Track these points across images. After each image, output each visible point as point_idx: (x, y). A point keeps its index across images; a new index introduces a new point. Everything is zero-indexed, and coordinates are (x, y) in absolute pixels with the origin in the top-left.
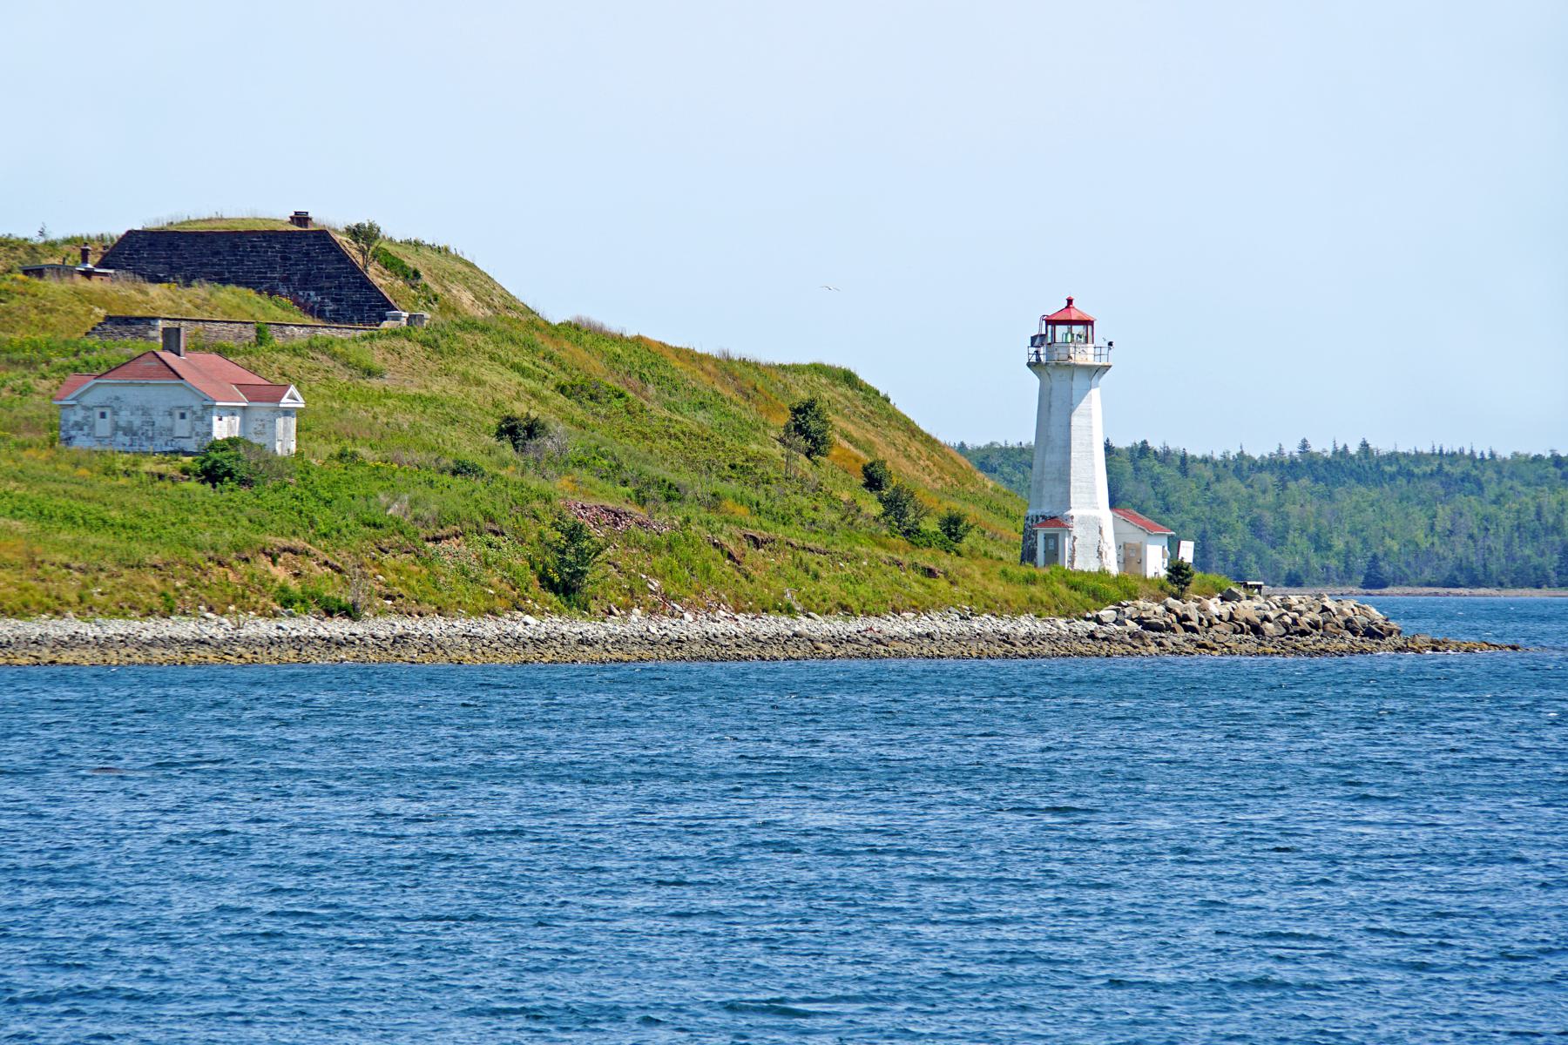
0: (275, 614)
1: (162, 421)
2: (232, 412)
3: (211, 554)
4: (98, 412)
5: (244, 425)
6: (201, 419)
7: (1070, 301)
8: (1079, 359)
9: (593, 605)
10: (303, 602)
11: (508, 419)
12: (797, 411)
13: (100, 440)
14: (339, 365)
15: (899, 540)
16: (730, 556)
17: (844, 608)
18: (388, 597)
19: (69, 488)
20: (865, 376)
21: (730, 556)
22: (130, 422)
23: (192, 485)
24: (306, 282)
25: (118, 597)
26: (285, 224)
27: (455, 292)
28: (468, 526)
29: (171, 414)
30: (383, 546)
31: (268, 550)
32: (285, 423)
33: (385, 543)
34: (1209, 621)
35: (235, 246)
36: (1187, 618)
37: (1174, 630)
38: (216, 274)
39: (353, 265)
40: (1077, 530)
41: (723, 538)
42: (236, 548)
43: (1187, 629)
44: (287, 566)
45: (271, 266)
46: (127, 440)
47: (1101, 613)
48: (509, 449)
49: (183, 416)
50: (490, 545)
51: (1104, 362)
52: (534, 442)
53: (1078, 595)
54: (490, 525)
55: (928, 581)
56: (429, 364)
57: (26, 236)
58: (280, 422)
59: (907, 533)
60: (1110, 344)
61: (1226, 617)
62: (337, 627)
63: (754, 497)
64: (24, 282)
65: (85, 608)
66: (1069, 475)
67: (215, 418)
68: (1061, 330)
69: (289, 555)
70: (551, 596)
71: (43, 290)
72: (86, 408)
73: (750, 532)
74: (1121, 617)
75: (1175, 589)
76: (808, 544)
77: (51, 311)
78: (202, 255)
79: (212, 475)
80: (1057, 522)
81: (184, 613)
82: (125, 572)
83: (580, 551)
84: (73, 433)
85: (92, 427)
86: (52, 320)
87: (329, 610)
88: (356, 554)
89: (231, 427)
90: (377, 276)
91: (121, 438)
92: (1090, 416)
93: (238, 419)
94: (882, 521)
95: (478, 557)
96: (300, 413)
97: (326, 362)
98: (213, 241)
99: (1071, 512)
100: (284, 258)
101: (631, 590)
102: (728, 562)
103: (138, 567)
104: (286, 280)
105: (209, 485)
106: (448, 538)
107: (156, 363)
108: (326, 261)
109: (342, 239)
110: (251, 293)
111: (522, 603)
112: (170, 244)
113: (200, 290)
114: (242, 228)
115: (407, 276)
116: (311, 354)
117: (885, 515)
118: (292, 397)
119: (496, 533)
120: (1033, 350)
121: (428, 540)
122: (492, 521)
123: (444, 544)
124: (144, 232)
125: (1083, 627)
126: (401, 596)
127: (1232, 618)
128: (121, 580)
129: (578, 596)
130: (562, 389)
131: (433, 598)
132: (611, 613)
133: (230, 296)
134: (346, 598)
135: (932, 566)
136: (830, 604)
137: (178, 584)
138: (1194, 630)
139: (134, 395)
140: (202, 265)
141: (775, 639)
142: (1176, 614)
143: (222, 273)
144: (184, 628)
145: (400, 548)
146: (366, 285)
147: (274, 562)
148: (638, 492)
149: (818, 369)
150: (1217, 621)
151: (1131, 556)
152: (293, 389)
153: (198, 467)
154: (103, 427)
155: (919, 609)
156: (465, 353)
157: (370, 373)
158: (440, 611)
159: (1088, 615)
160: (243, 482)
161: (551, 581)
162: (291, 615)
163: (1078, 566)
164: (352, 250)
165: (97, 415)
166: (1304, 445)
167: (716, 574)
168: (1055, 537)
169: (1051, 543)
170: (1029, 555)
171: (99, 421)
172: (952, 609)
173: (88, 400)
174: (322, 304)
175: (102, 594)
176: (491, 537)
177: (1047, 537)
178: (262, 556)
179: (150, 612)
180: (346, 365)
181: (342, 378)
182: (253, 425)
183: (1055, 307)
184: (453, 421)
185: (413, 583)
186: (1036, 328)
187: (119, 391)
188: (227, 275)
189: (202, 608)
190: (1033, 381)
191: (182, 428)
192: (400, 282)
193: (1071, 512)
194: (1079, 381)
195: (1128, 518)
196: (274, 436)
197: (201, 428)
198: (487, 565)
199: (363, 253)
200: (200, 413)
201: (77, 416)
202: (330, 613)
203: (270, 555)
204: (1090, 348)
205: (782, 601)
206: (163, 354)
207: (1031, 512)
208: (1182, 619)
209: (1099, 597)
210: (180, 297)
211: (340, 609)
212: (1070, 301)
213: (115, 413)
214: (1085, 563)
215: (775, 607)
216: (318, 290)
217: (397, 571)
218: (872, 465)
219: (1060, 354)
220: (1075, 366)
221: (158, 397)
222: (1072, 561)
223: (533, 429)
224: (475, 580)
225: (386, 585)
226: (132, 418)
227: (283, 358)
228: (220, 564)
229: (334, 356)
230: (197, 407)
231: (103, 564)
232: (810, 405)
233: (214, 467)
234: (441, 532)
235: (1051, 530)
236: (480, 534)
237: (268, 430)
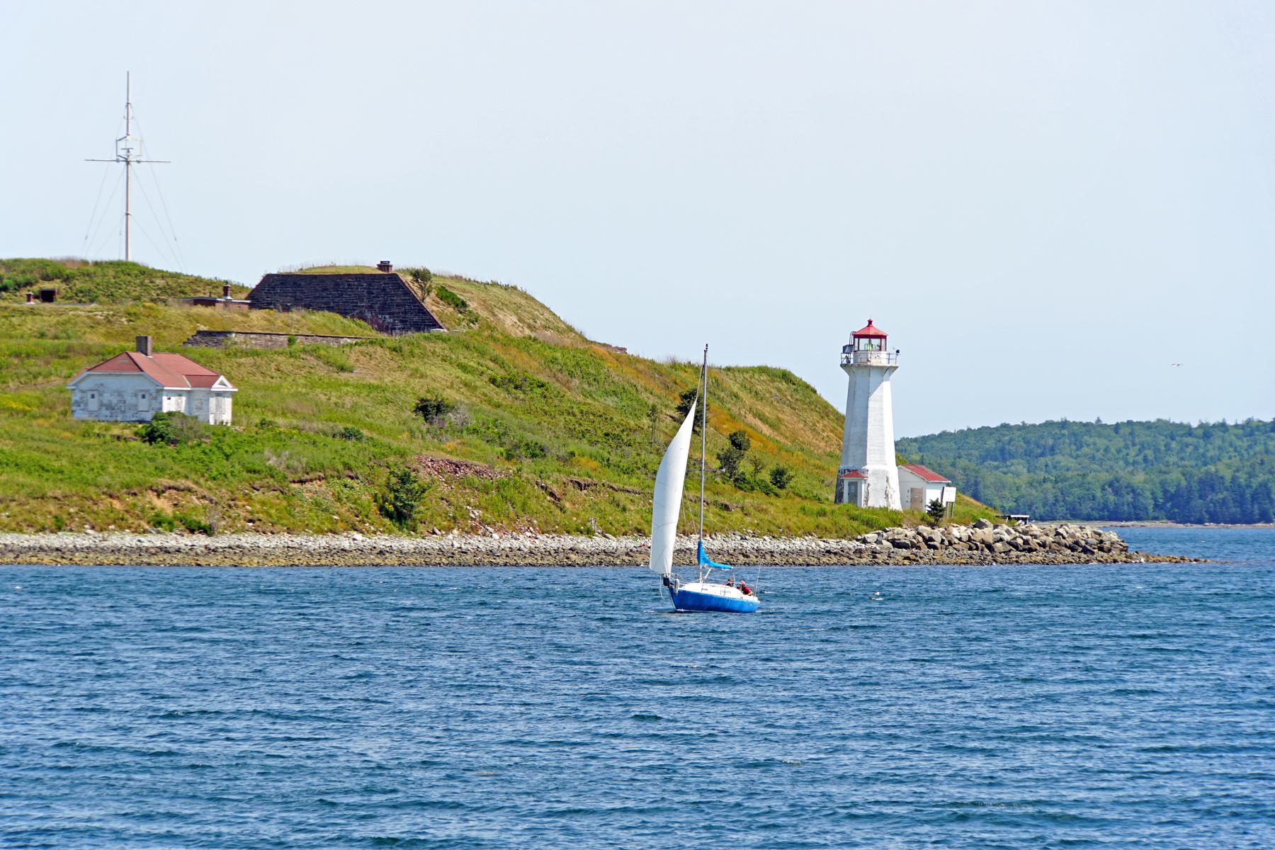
0: (145, 531)
1: (130, 400)
2: (179, 394)
3: (105, 490)
4: (89, 394)
5: (189, 403)
6: (155, 398)
7: (870, 322)
8: (874, 362)
9: (421, 527)
10: (170, 523)
11: (422, 400)
13: (91, 413)
14: (321, 363)
15: (729, 487)
16: (552, 494)
18: (250, 521)
19: (41, 444)
20: (798, 372)
21: (552, 494)
22: (110, 401)
23: (137, 444)
24: (384, 309)
25: (20, 518)
26: (373, 269)
27: (500, 316)
28: (329, 472)
29: (136, 395)
30: (256, 486)
31: (155, 488)
32: (218, 401)
34: (950, 542)
35: (337, 284)
36: (931, 539)
37: (919, 548)
38: (325, 303)
39: (414, 300)
40: (870, 480)
41: (549, 482)
45: (360, 298)
46: (108, 413)
47: (866, 536)
48: (422, 419)
49: (143, 397)
50: (345, 486)
51: (892, 364)
52: (441, 416)
53: (855, 524)
55: (725, 513)
56: (392, 363)
57: (226, 279)
58: (213, 401)
59: (736, 480)
60: (898, 352)
61: (965, 539)
62: (201, 541)
64: (150, 308)
66: (866, 441)
67: (165, 398)
68: (864, 341)
70: (387, 521)
71: (163, 313)
72: (83, 391)
73: (576, 478)
74: (880, 539)
75: (932, 520)
77: (165, 327)
78: (316, 291)
79: (151, 437)
80: (857, 474)
81: (71, 530)
83: (409, 491)
84: (74, 408)
85: (86, 404)
86: (165, 334)
87: (193, 529)
88: (232, 492)
89: (178, 404)
91: (105, 412)
92: (882, 401)
93: (184, 399)
94: (719, 472)
95: (333, 494)
96: (232, 395)
98: (323, 281)
99: (867, 467)
101: (454, 518)
102: (549, 498)
103: (42, 498)
104: (370, 308)
105: (147, 444)
106: (311, 480)
107: (127, 361)
108: (397, 295)
109: (408, 279)
110: (338, 317)
112: (295, 283)
113: (295, 315)
114: (343, 272)
115: (457, 305)
116: (302, 356)
117: (721, 468)
118: (222, 384)
119: (352, 478)
120: (844, 355)
121: (294, 482)
122: (350, 469)
123: (308, 485)
125: (854, 544)
126: (260, 520)
127: (970, 539)
128: (27, 507)
129: (409, 522)
130: (493, 381)
131: (285, 522)
132: (434, 533)
133: (321, 319)
134: (204, 522)
135: (728, 503)
136: (627, 528)
137: (72, 510)
139: (113, 383)
140: (316, 298)
141: (131, 550)
142: (923, 537)
143: (329, 303)
144: (64, 540)
145: (269, 487)
146: (422, 311)
149: (763, 370)
150: (957, 541)
151: (914, 497)
152: (222, 378)
153: (144, 432)
154: (93, 405)
156: (423, 356)
157: (342, 369)
158: (289, 531)
159: (859, 537)
160: (174, 442)
161: (387, 511)
162: (159, 532)
163: (870, 504)
164: (415, 288)
165: (89, 396)
166: (1099, 420)
169: (853, 488)
170: (839, 497)
171: (91, 400)
172: (737, 532)
173: (83, 386)
174: (393, 324)
175: (8, 517)
176: (349, 481)
177: (850, 484)
178: (150, 492)
179: (43, 529)
182: (196, 403)
183: (860, 326)
184: (388, 402)
185: (273, 511)
186: (847, 340)
188: (332, 304)
189: (87, 526)
190: (845, 377)
191: (143, 404)
192: (451, 309)
193: (867, 467)
194: (874, 377)
196: (208, 410)
198: (339, 500)
199: (421, 288)
200: (154, 395)
201: (76, 397)
202: (192, 531)
203: (156, 491)
204: (883, 354)
205: (585, 525)
206: (134, 355)
207: (842, 467)
210: (276, 319)
211: (200, 528)
212: (870, 322)
213: (101, 395)
214: (876, 501)
216: (391, 314)
217: (263, 503)
218: (735, 434)
220: (871, 366)
221: (128, 384)
222: (867, 501)
223: (440, 408)
225: (251, 513)
226: (111, 398)
227: (280, 359)
228: (111, 496)
229: (319, 357)
230: (152, 389)
231: (16, 497)
233: (153, 432)
234: (307, 477)
236: (339, 478)
237: (204, 406)
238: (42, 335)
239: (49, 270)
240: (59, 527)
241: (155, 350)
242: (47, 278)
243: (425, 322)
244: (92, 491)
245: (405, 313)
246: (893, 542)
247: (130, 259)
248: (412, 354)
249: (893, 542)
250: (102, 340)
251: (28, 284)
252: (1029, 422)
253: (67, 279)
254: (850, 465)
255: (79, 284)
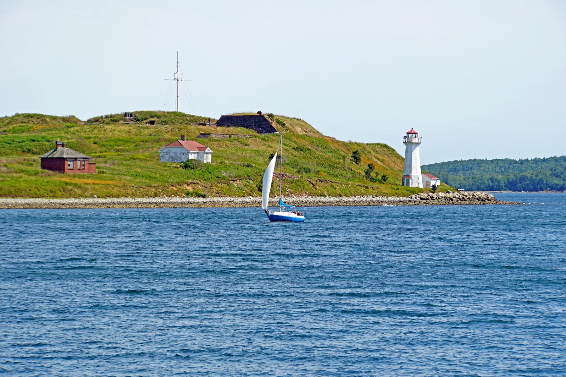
1: (179, 155)
5: (198, 156)
7: (412, 129)
8: (414, 141)
12: (354, 153)
13: (166, 159)
15: (368, 181)
17: (340, 195)
21: (312, 184)
23: (181, 169)
24: (259, 126)
33: (219, 181)
36: (433, 197)
40: (413, 178)
42: (178, 183)
43: (432, 199)
44: (192, 186)
46: (172, 159)
51: (419, 142)
53: (408, 192)
54: (248, 178)
55: (367, 189)
58: (205, 155)
62: (201, 200)
63: (329, 171)
65: (133, 195)
68: (410, 135)
69: (193, 184)
72: (164, 153)
75: (433, 191)
76: (336, 181)
79: (186, 167)
80: (409, 177)
82: (147, 188)
87: (199, 196)
89: (194, 157)
90: (274, 125)
91: (171, 159)
93: (196, 155)
96: (212, 153)
97: (237, 143)
100: (255, 121)
104: (255, 126)
107: (178, 143)
111: (252, 194)
113: (231, 128)
114: (246, 115)
118: (208, 150)
122: (249, 176)
123: (236, 182)
124: (226, 116)
125: (408, 199)
130: (294, 148)
134: (203, 194)
136: (336, 194)
138: (434, 200)
147: (188, 186)
148: (298, 170)
149: (378, 144)
151: (427, 184)
152: (208, 148)
153: (183, 165)
154: (167, 157)
155: (362, 195)
157: (246, 145)
160: (193, 168)
164: (269, 120)
167: (306, 187)
168: (408, 180)
170: (403, 184)
171: (183, 156)
173: (164, 151)
179: (151, 197)
180: (241, 143)
181: (240, 146)
182: (200, 156)
185: (224, 190)
187: (170, 149)
191: (183, 157)
194: (414, 146)
195: (424, 176)
197: (187, 157)
201: (162, 154)
202: (199, 197)
204: (416, 139)
208: (432, 197)
209: (413, 193)
212: (412, 129)
214: (415, 185)
215: (321, 195)
216: (262, 128)
217: (221, 188)
219: (410, 140)
221: (178, 150)
224: (241, 189)
229: (239, 141)
230: (186, 153)
232: (356, 152)
234: (235, 179)
235: (407, 178)
236: (245, 179)
238: (151, 135)
239: (153, 114)
240: (156, 196)
241: (187, 140)
242: (152, 117)
243: (272, 130)
244: (167, 184)
245: (266, 127)
246: (420, 198)
247: (179, 111)
248: (268, 140)
249: (420, 198)
250: (170, 137)
251: (146, 119)
252: (463, 160)
253: (158, 117)
254: (406, 174)
255: (162, 119)
